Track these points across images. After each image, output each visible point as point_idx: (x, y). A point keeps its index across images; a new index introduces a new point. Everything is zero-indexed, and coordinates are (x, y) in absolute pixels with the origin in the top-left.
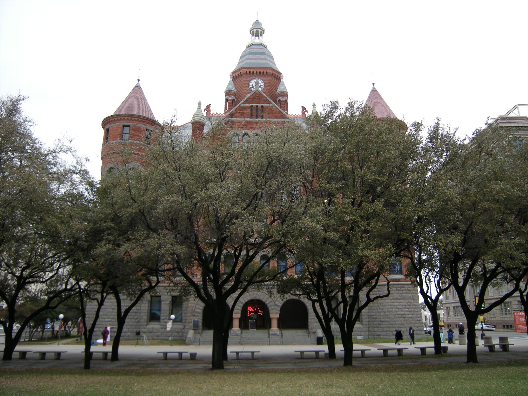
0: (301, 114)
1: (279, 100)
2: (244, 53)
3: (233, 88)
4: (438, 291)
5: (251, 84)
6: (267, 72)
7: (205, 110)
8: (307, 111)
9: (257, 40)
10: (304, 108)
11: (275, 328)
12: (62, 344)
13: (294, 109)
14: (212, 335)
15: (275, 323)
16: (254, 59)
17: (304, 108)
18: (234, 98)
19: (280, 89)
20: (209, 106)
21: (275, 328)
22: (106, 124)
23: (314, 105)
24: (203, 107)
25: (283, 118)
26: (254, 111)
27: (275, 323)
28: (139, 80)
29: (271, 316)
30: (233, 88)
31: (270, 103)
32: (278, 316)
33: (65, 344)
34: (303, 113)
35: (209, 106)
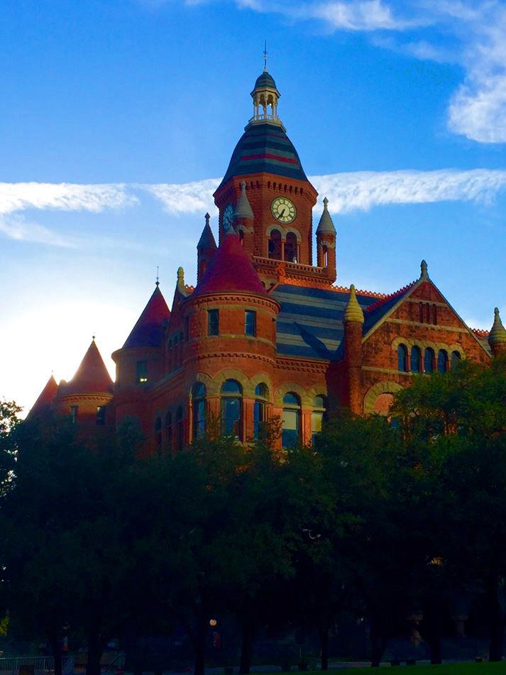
6: (302, 189)
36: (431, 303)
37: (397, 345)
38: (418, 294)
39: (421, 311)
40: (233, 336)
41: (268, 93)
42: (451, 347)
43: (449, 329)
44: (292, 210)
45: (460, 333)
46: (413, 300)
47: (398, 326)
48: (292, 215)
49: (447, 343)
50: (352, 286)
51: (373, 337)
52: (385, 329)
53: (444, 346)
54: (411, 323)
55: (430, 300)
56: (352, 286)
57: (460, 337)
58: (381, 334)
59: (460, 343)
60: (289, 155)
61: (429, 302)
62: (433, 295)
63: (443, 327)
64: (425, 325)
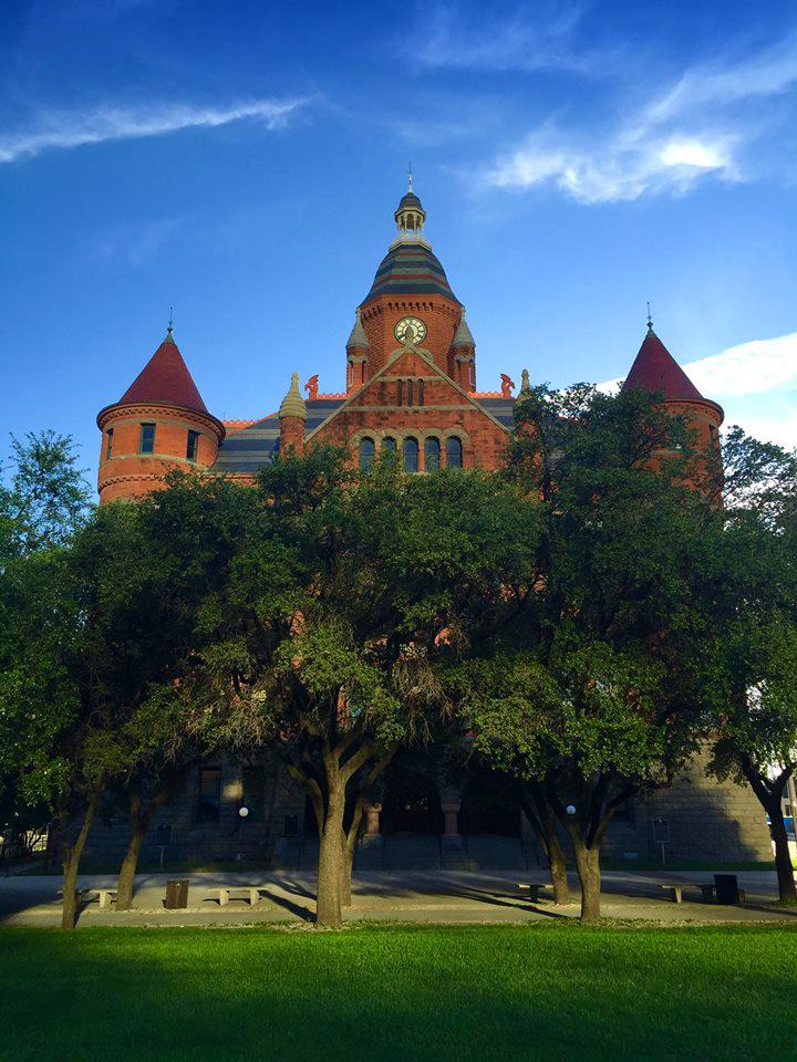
0: (500, 391)
1: (458, 361)
2: (384, 266)
3: (363, 340)
4: (784, 767)
5: (400, 329)
6: (431, 304)
7: (307, 386)
8: (512, 385)
9: (408, 237)
10: (505, 379)
11: (452, 834)
12: (16, 875)
13: (487, 384)
14: (777, 877)
15: (451, 822)
16: (405, 277)
17: (505, 379)
18: (366, 359)
19: (461, 338)
20: (314, 380)
21: (452, 834)
22: (103, 425)
23: (525, 375)
24: (303, 381)
25: (462, 403)
26: (416, 395)
27: (451, 822)
28: (170, 330)
29: (445, 807)
30: (363, 340)
31: (434, 373)
32: (457, 807)
33: (20, 875)
34: (505, 390)
35: (314, 380)
36: (415, 379)
37: (359, 439)
38: (395, 370)
39: (400, 389)
40: (123, 457)
41: (406, 214)
42: (446, 431)
43: (444, 408)
44: (421, 328)
45: (463, 411)
46: (386, 379)
47: (361, 414)
48: (422, 334)
49: (439, 428)
50: (654, 364)
51: (322, 435)
52: (342, 421)
53: (434, 432)
54: (382, 408)
55: (414, 374)
56: (654, 364)
57: (462, 417)
58: (334, 428)
59: (461, 424)
60: (441, 278)
61: (412, 377)
62: (418, 369)
63: (433, 407)
64: (405, 407)
